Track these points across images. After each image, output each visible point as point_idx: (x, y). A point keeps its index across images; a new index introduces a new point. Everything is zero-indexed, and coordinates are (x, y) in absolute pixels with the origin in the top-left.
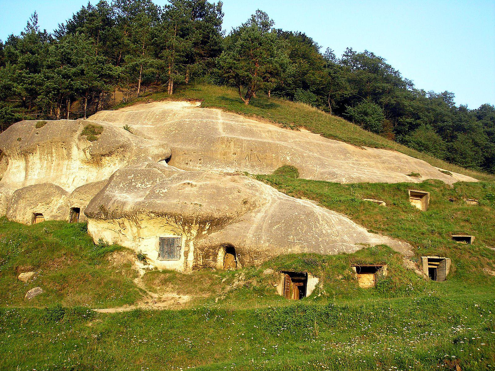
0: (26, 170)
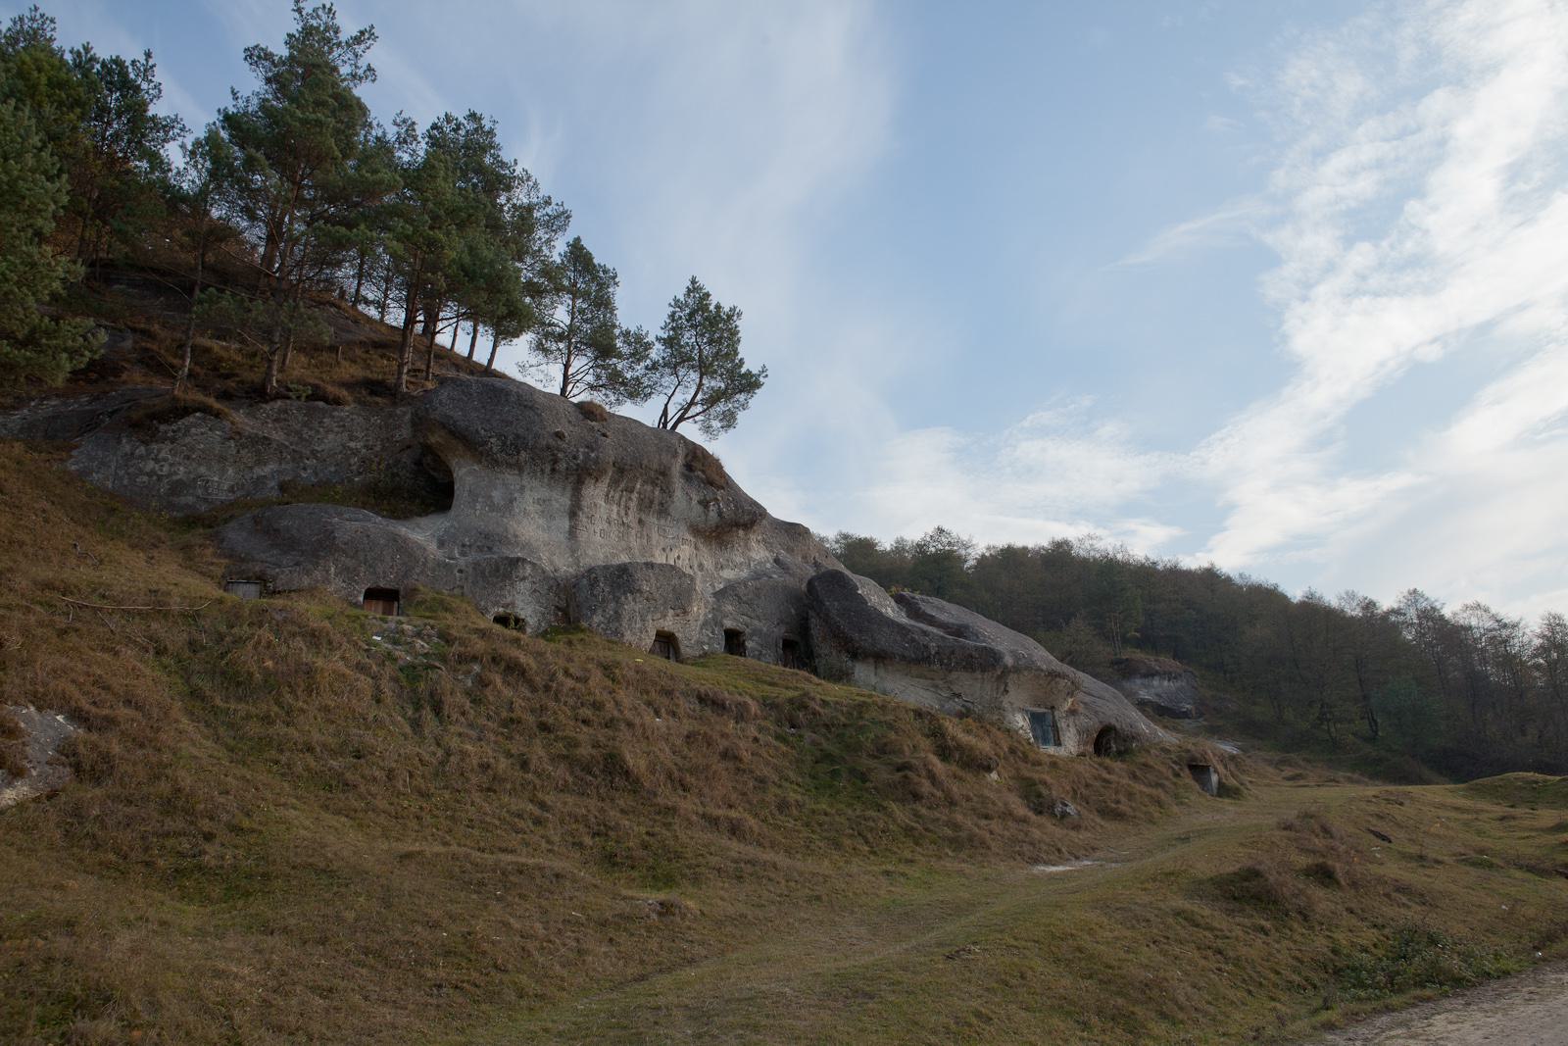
0: (573, 514)
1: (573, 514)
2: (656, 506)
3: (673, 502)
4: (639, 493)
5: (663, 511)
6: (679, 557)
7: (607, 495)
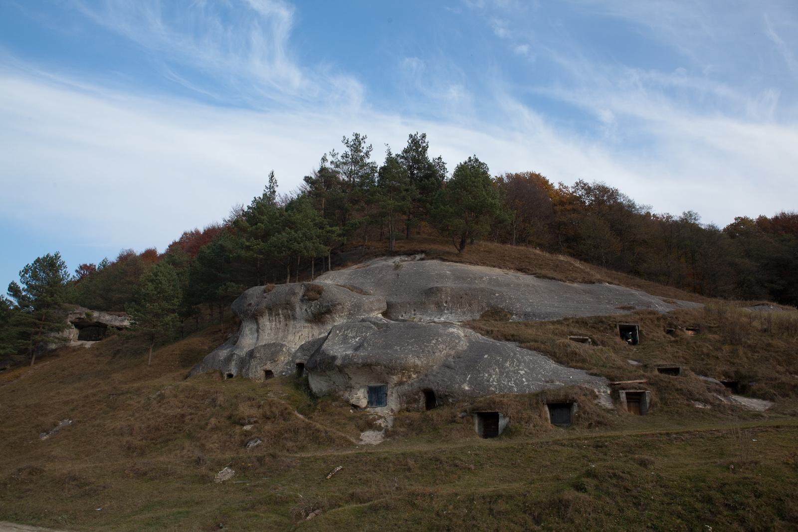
1: (258, 331)
2: (291, 317)
3: (296, 313)
4: (282, 314)
5: (294, 318)
6: (302, 335)
7: (269, 320)
